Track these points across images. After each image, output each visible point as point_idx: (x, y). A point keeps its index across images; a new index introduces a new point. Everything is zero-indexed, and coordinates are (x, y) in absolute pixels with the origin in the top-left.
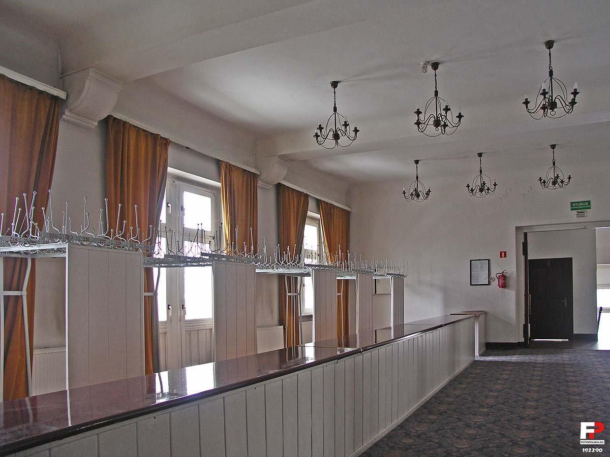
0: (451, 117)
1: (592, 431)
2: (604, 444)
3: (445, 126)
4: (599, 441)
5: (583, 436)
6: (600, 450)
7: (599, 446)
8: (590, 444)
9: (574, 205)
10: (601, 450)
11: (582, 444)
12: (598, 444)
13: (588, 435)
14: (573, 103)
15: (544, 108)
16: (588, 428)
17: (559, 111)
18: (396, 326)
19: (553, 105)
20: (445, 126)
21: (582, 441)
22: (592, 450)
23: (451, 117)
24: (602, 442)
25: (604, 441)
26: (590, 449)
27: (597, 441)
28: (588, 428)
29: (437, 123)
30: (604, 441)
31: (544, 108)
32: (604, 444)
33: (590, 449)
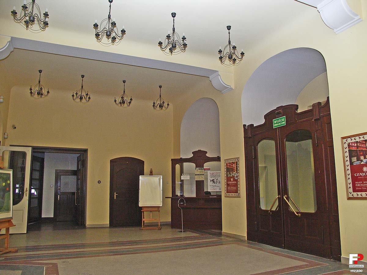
0: (44, 91)
1: (356, 259)
2: (363, 267)
3: (42, 94)
4: (360, 265)
5: (351, 262)
6: (361, 271)
7: (360, 269)
8: (355, 267)
9: (302, 152)
10: (361, 271)
11: (350, 267)
12: (360, 267)
13: (355, 262)
14: (130, 103)
15: (120, 103)
16: (354, 257)
17: (125, 105)
18: (9, 192)
19: (124, 102)
20: (42, 94)
21: (350, 265)
22: (356, 271)
23: (165, 104)
24: (363, 266)
25: (363, 265)
26: (355, 270)
27: (359, 265)
28: (354, 257)
29: (38, 94)
30: (363, 265)
31: (120, 103)
32: (363, 267)
33: (355, 270)
